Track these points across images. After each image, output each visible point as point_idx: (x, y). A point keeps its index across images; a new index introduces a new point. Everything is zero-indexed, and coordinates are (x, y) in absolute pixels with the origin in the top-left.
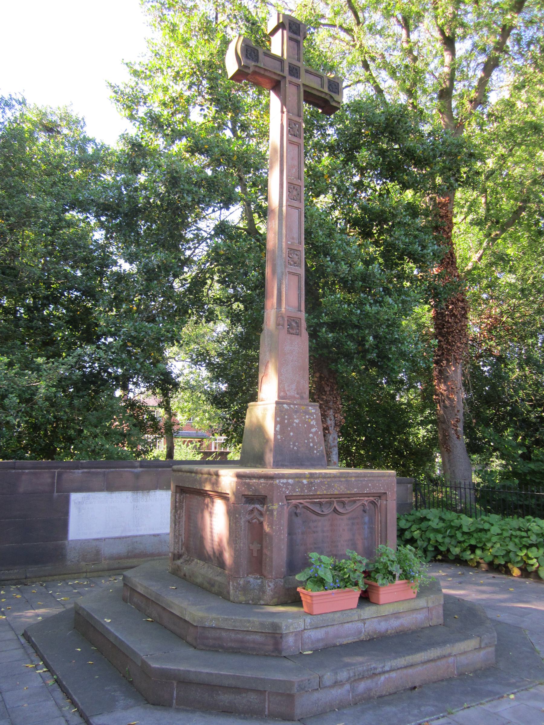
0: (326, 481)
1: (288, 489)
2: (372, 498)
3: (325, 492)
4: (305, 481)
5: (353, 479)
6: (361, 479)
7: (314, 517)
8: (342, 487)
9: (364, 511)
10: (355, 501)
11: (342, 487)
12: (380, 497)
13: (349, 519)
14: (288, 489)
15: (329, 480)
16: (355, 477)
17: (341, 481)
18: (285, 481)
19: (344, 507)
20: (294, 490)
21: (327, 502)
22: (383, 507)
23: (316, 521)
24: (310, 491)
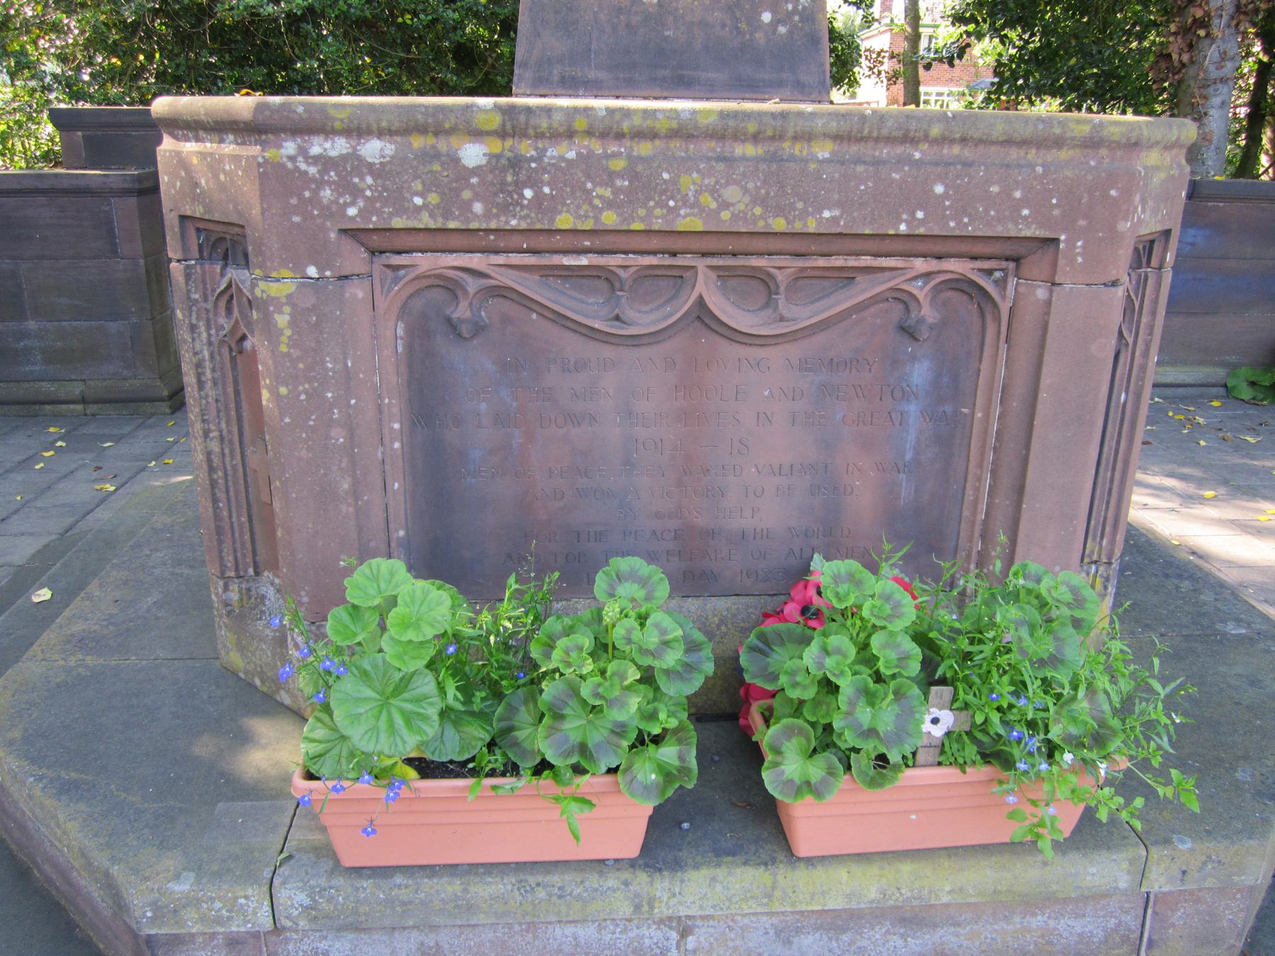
0: (618, 156)
1: (356, 192)
2: (956, 266)
3: (610, 219)
4: (473, 154)
5: (823, 151)
6: (885, 152)
7: (574, 346)
8: (732, 193)
9: (908, 331)
10: (847, 277)
11: (732, 193)
12: (1017, 260)
13: (805, 366)
14: (356, 192)
15: (645, 149)
16: (837, 138)
17: (728, 160)
18: (338, 147)
19: (769, 302)
20: (400, 204)
21: (648, 274)
22: (1027, 320)
23: (580, 365)
24: (505, 209)
